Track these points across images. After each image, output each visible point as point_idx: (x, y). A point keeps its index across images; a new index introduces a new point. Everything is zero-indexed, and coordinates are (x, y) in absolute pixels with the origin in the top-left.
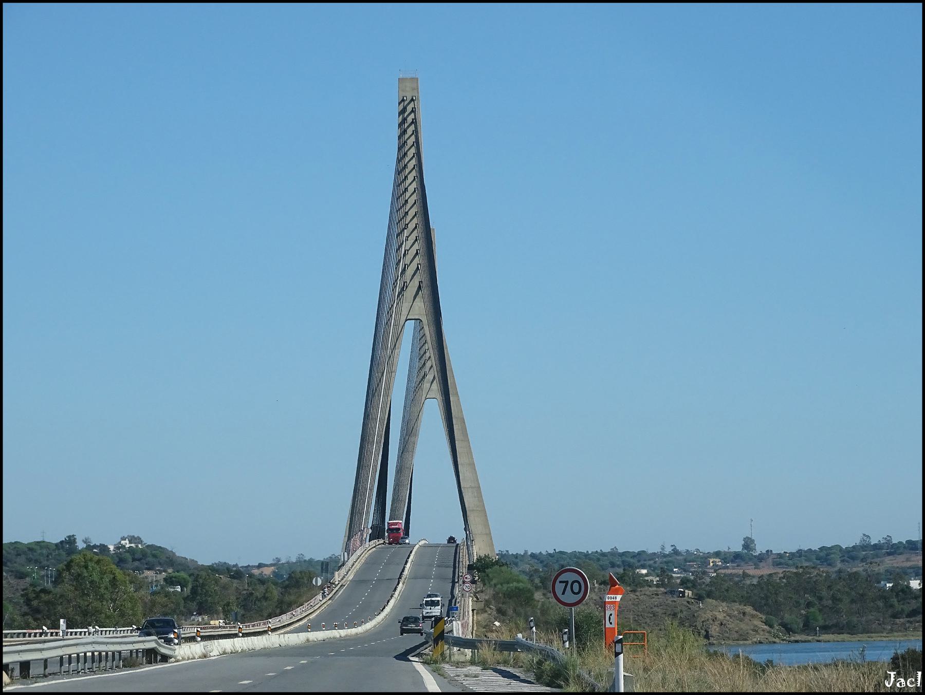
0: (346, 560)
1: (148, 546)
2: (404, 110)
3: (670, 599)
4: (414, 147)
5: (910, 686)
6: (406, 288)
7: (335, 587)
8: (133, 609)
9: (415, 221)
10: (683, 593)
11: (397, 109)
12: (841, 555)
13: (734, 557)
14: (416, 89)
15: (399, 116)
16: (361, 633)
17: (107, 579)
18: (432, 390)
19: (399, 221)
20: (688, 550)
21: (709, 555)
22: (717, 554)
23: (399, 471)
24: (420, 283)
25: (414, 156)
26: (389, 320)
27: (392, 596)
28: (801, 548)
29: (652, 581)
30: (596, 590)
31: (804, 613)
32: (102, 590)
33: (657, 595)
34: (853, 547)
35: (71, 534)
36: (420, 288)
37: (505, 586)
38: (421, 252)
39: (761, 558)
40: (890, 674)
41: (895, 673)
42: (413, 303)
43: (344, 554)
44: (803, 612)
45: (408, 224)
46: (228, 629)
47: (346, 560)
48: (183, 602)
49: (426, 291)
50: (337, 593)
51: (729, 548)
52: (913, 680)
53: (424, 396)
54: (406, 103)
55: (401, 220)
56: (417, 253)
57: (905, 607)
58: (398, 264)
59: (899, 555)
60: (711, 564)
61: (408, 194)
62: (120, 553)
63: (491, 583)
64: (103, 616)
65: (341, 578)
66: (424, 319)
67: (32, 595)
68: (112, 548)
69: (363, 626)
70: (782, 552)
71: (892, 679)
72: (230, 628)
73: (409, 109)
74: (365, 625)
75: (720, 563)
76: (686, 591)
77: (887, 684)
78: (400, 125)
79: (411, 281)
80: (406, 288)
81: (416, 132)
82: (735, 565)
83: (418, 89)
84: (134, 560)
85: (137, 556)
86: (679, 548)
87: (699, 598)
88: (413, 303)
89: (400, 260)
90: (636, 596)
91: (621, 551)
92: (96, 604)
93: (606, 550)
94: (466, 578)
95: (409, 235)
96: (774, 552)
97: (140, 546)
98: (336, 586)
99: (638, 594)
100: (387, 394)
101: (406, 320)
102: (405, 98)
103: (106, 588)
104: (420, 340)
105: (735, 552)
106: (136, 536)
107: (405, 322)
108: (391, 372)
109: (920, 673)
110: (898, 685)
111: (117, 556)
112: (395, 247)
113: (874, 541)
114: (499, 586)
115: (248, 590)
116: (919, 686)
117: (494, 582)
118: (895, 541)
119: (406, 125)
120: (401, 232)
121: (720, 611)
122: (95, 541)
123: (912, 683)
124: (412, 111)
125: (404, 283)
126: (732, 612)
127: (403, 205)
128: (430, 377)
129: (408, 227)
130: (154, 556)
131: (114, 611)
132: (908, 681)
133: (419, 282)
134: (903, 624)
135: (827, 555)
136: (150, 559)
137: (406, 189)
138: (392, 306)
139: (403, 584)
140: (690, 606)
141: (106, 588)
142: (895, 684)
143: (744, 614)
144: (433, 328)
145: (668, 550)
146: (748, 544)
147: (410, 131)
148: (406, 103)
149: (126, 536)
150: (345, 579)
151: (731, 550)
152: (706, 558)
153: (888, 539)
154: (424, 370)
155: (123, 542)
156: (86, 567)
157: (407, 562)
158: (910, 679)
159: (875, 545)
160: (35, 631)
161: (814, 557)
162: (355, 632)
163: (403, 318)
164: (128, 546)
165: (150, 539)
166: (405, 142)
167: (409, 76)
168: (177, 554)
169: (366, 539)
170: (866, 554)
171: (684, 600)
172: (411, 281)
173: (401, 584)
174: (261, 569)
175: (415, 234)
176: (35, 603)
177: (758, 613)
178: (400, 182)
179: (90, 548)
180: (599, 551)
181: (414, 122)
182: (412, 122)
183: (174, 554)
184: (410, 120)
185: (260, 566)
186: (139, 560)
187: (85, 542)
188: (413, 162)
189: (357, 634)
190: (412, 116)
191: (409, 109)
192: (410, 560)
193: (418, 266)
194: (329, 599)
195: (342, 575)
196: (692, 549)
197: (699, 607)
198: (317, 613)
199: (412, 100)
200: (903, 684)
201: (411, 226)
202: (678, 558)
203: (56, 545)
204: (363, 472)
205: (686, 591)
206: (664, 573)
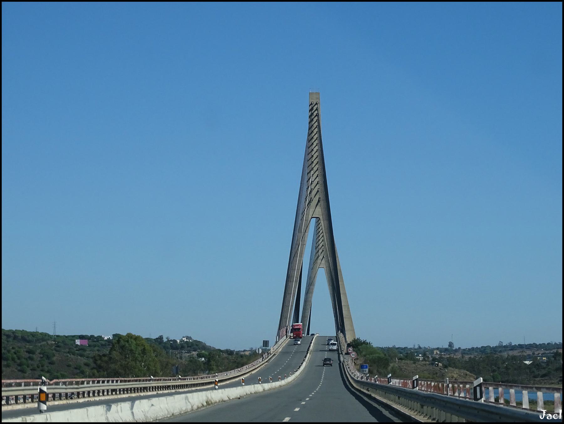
0: (278, 340)
1: (194, 341)
3: (431, 367)
4: (317, 128)
6: (312, 201)
7: (270, 355)
8: (155, 366)
9: (317, 154)
10: (438, 364)
11: (308, 108)
12: (490, 350)
13: (445, 350)
14: (319, 98)
15: (309, 112)
16: (284, 385)
17: (140, 348)
18: (322, 264)
19: (309, 167)
20: (425, 347)
21: (434, 349)
22: (438, 349)
23: (305, 301)
25: (317, 133)
26: (303, 212)
27: (304, 360)
28: (473, 347)
29: (419, 359)
30: (397, 362)
31: (492, 375)
32: (137, 355)
33: (425, 365)
34: (496, 347)
35: (161, 335)
36: (319, 201)
37: (371, 356)
38: (320, 182)
39: (456, 351)
41: (546, 411)
43: (276, 337)
44: (492, 374)
45: (313, 168)
46: (23, 388)
47: (278, 340)
48: (203, 365)
49: (322, 203)
50: (270, 359)
51: (443, 346)
54: (313, 105)
55: (310, 165)
56: (318, 183)
57: (539, 372)
58: (308, 189)
59: (515, 350)
60: (435, 353)
61: (313, 152)
62: (182, 344)
63: (362, 354)
64: (137, 370)
65: (274, 350)
66: (321, 217)
67: (98, 358)
68: (178, 341)
69: (286, 380)
70: (465, 348)
71: (544, 415)
72: (25, 386)
73: (315, 108)
74: (287, 379)
75: (439, 353)
76: (439, 364)
79: (314, 197)
80: (312, 201)
81: (318, 121)
82: (445, 353)
83: (319, 98)
84: (188, 347)
85: (190, 345)
86: (421, 346)
87: (445, 367)
89: (310, 178)
90: (416, 365)
91: (397, 347)
92: (133, 363)
93: (391, 346)
94: (349, 350)
96: (462, 348)
97: (191, 341)
98: (271, 354)
99: (416, 364)
100: (301, 256)
102: (313, 103)
103: (139, 354)
104: (316, 239)
105: (445, 348)
106: (189, 336)
107: (311, 219)
108: (303, 245)
110: (548, 418)
111: (181, 345)
112: (306, 180)
114: (368, 356)
115: (234, 360)
117: (364, 353)
119: (313, 134)
120: (310, 172)
121: (455, 373)
122: (172, 338)
124: (316, 110)
125: (311, 198)
126: (460, 374)
127: (311, 164)
128: (321, 257)
130: (197, 345)
131: (145, 367)
132: (554, 415)
133: (319, 198)
134: (539, 380)
135: (484, 350)
136: (195, 346)
137: (312, 150)
138: (304, 210)
139: (310, 354)
140: (441, 370)
141: (139, 354)
143: (466, 375)
144: (326, 222)
145: (417, 347)
146: (451, 345)
147: (315, 120)
149: (185, 336)
150: (276, 351)
151: (443, 347)
152: (433, 350)
153: (510, 344)
155: (183, 339)
156: (128, 341)
157: (311, 343)
159: (505, 346)
160: (98, 379)
161: (479, 350)
162: (279, 385)
163: (310, 217)
164: (185, 340)
165: (196, 337)
166: (313, 125)
167: (314, 91)
168: (207, 344)
169: (289, 331)
170: (501, 350)
171: (439, 368)
172: (314, 197)
173: (309, 354)
174: (245, 352)
175: (317, 173)
176: (99, 362)
177: (473, 375)
179: (169, 341)
180: (387, 347)
181: (317, 115)
182: (316, 115)
183: (205, 344)
184: (315, 114)
185: (244, 351)
186: (190, 347)
187: (167, 338)
188: (316, 130)
189: (280, 386)
190: (316, 118)
191: (315, 108)
192: (313, 342)
194: (266, 362)
195: (275, 349)
196: (427, 347)
197: (445, 371)
198: (258, 370)
199: (316, 104)
201: (315, 169)
202: (421, 350)
203: (155, 340)
204: (288, 296)
205: (439, 364)
206: (424, 355)
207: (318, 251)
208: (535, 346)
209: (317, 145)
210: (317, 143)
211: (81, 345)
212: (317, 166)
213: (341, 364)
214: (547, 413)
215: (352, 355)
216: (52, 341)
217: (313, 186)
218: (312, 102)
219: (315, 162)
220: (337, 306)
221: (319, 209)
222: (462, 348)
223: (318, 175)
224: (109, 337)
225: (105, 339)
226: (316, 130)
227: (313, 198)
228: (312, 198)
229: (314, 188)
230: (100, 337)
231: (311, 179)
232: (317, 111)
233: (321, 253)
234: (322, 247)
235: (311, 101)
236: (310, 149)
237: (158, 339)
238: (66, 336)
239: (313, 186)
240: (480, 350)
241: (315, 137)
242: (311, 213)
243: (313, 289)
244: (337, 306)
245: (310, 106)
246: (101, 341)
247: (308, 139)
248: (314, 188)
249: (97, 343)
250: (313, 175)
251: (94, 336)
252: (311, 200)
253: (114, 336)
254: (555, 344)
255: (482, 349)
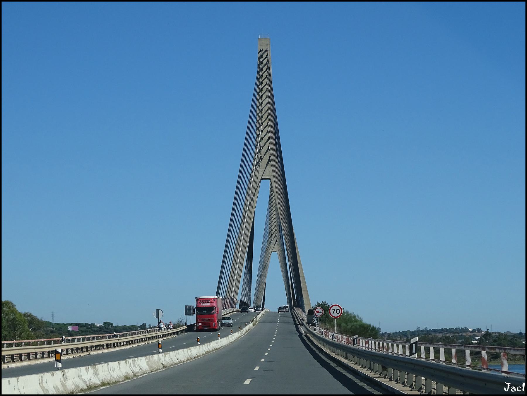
2: (261, 56)
4: (267, 78)
5: (518, 391)
6: (262, 160)
24: (269, 147)
25: (267, 84)
28: (396, 331)
34: (414, 331)
36: (269, 160)
40: (507, 384)
41: (510, 383)
42: (265, 168)
45: (263, 123)
52: (520, 388)
53: (271, 251)
54: (262, 53)
56: (268, 140)
61: (263, 105)
71: (508, 387)
73: (264, 56)
77: (505, 390)
78: (259, 66)
79: (264, 156)
80: (262, 160)
81: (268, 70)
88: (265, 168)
94: (318, 312)
95: (264, 130)
101: (262, 179)
109: (524, 384)
110: (512, 390)
113: (421, 329)
116: (523, 391)
118: (428, 329)
119: (263, 85)
123: (519, 389)
124: (266, 57)
125: (260, 157)
128: (274, 242)
129: (263, 125)
132: (518, 388)
135: (406, 333)
137: (262, 103)
142: (510, 389)
147: (264, 69)
148: (262, 53)
153: (426, 329)
154: (271, 238)
158: (519, 387)
159: (422, 330)
161: (401, 334)
163: (260, 178)
172: (264, 156)
178: (258, 90)
182: (266, 64)
184: (264, 62)
190: (266, 67)
191: (264, 56)
193: (269, 147)
199: (266, 51)
200: (514, 390)
201: (265, 124)
207: (271, 236)
208: (446, 331)
209: (267, 97)
210: (267, 95)
211: (72, 331)
212: (267, 121)
213: (303, 336)
214: (511, 386)
215: (332, 311)
216: (51, 328)
217: (262, 143)
218: (261, 49)
219: (265, 116)
220: (292, 298)
221: (269, 169)
222: (388, 332)
223: (268, 130)
224: (101, 324)
225: (97, 326)
226: (266, 80)
227: (263, 157)
228: (262, 156)
229: (264, 145)
230: (93, 324)
231: (260, 136)
232: (267, 59)
233: (274, 238)
234: (274, 232)
235: (260, 48)
236: (259, 102)
237: (142, 326)
238: (65, 324)
239: (262, 143)
240: (402, 334)
241: (264, 76)
242: (260, 174)
243: (266, 272)
244: (292, 298)
245: (259, 53)
246: (93, 327)
247: (256, 83)
248: (264, 145)
249: (89, 329)
250: (263, 130)
251: (88, 324)
252: (260, 158)
253: (105, 323)
254: (462, 328)
255: (404, 333)
